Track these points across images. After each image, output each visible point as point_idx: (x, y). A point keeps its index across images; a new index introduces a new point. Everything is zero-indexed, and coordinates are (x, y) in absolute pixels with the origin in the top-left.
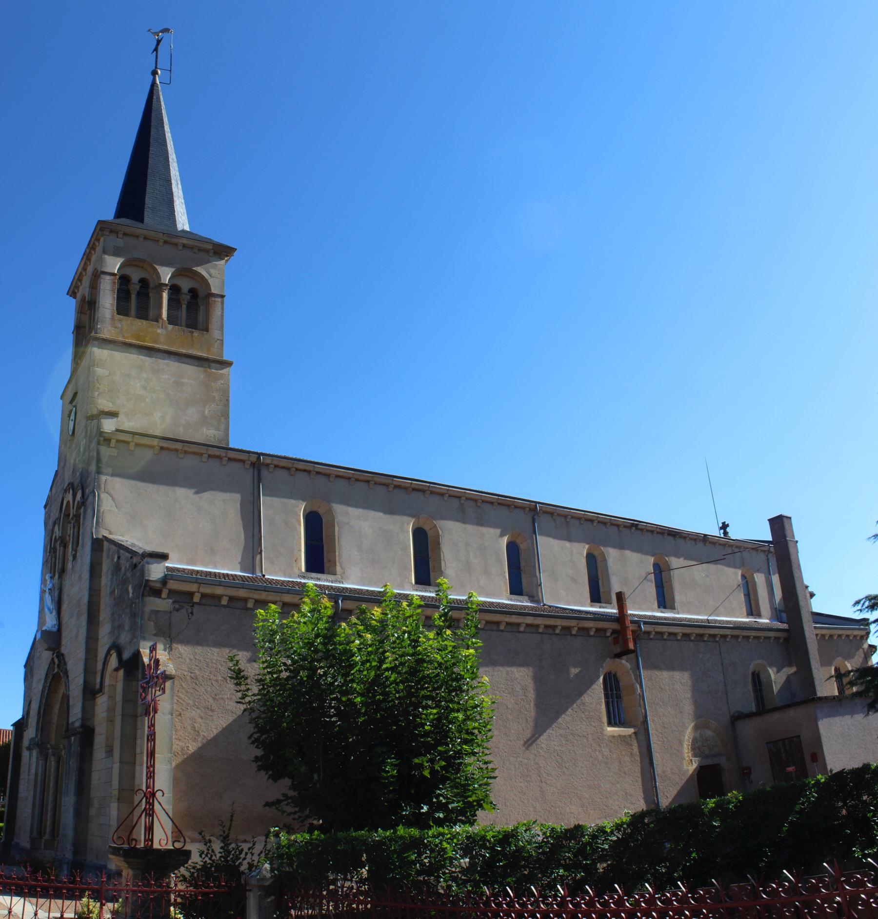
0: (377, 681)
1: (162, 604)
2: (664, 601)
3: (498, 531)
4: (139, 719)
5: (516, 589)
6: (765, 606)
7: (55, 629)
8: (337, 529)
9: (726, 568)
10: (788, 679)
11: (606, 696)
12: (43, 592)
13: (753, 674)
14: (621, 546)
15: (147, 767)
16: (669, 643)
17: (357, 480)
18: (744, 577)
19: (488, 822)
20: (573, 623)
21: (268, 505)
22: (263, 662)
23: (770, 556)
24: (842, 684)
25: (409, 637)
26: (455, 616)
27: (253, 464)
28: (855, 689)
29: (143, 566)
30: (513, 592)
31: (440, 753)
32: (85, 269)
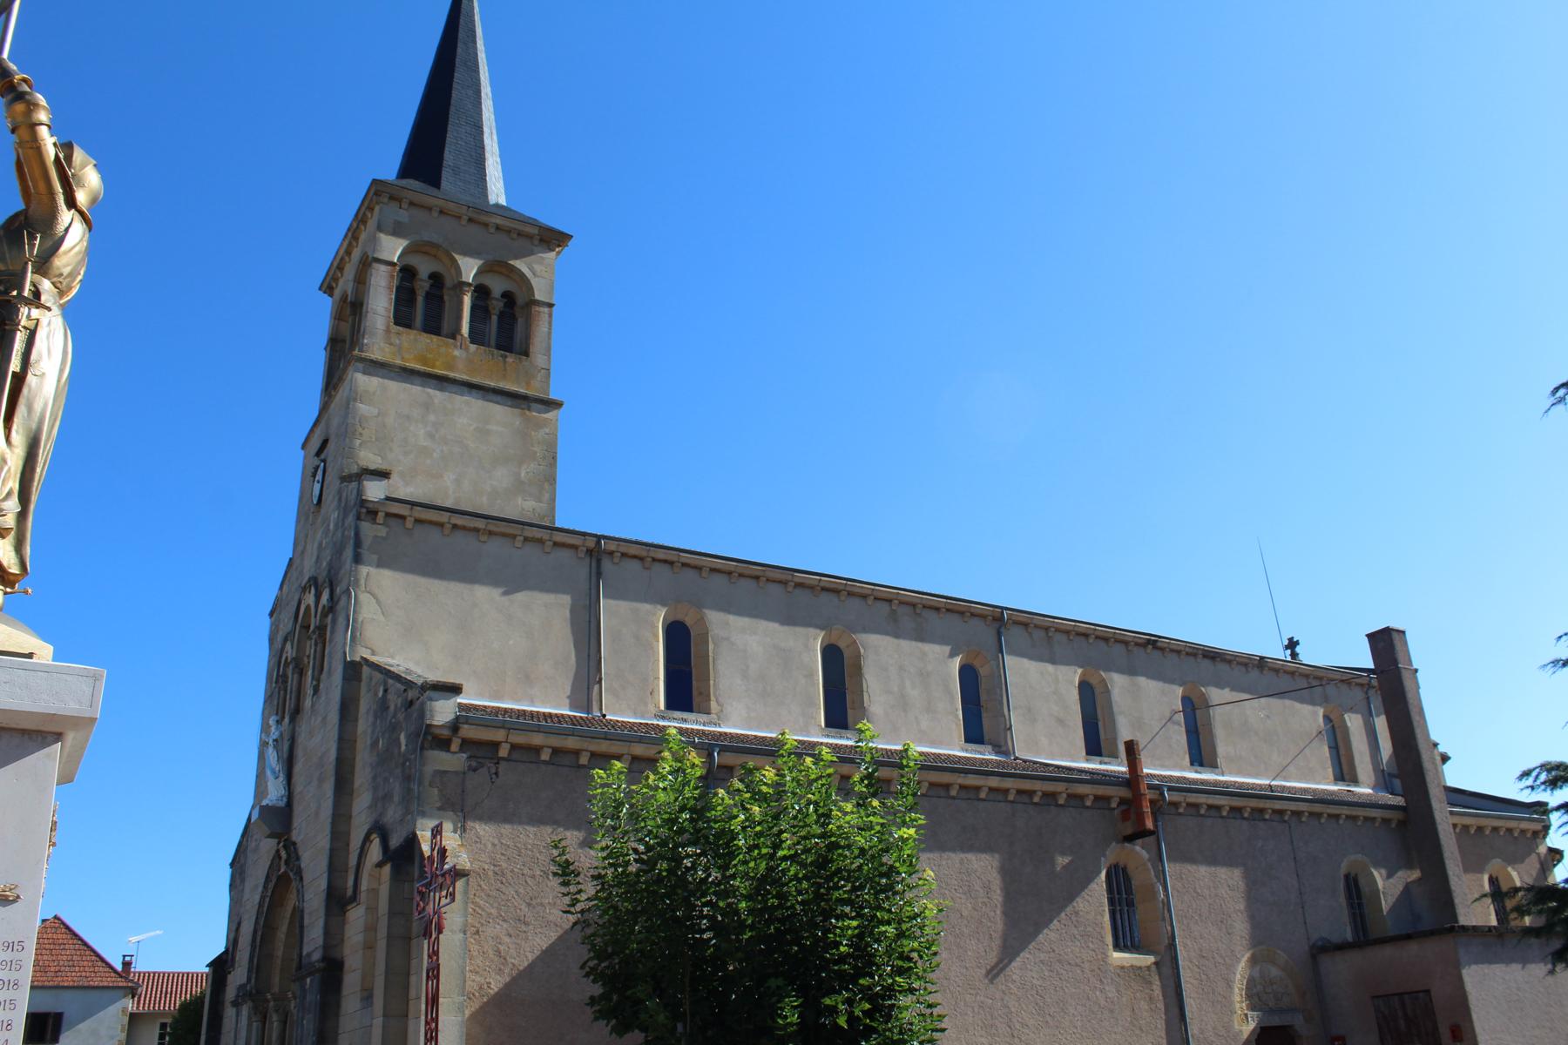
0: (770, 879)
1: (451, 761)
2: (1201, 754)
3: (947, 649)
4: (414, 942)
5: (974, 735)
6: (1364, 767)
7: (282, 804)
8: (711, 647)
9: (1298, 705)
11: (1111, 902)
12: (263, 745)
13: (1347, 877)
14: (1131, 671)
15: (427, 1023)
16: (1208, 822)
17: (741, 575)
18: (1327, 718)
20: (1060, 787)
21: (611, 612)
22: (603, 849)
23: (1371, 692)
24: (1504, 907)
25: (816, 811)
26: (884, 777)
27: (590, 552)
28: (1527, 920)
29: (423, 704)
31: (863, 989)
32: (348, 252)
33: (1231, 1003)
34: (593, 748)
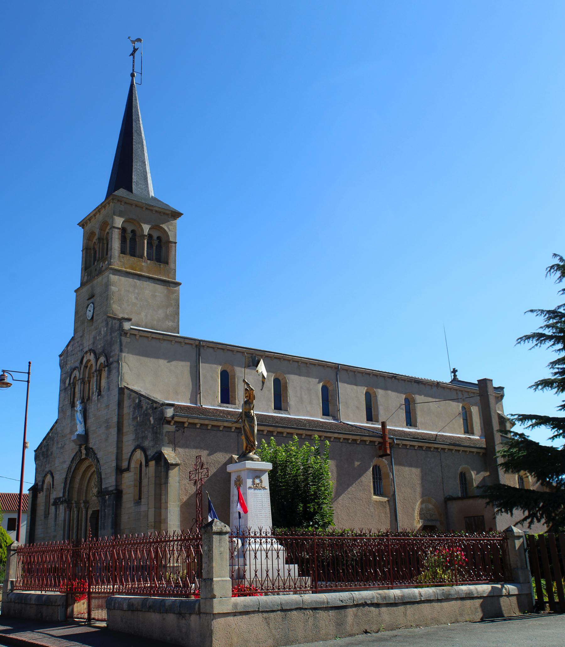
1: (170, 428)
2: (411, 421)
3: (318, 380)
5: (326, 413)
7: (84, 433)
8: (236, 380)
10: (484, 478)
11: (374, 478)
13: (461, 473)
14: (386, 388)
16: (410, 451)
18: (463, 408)
20: (358, 438)
21: (204, 368)
27: (196, 346)
33: (414, 516)
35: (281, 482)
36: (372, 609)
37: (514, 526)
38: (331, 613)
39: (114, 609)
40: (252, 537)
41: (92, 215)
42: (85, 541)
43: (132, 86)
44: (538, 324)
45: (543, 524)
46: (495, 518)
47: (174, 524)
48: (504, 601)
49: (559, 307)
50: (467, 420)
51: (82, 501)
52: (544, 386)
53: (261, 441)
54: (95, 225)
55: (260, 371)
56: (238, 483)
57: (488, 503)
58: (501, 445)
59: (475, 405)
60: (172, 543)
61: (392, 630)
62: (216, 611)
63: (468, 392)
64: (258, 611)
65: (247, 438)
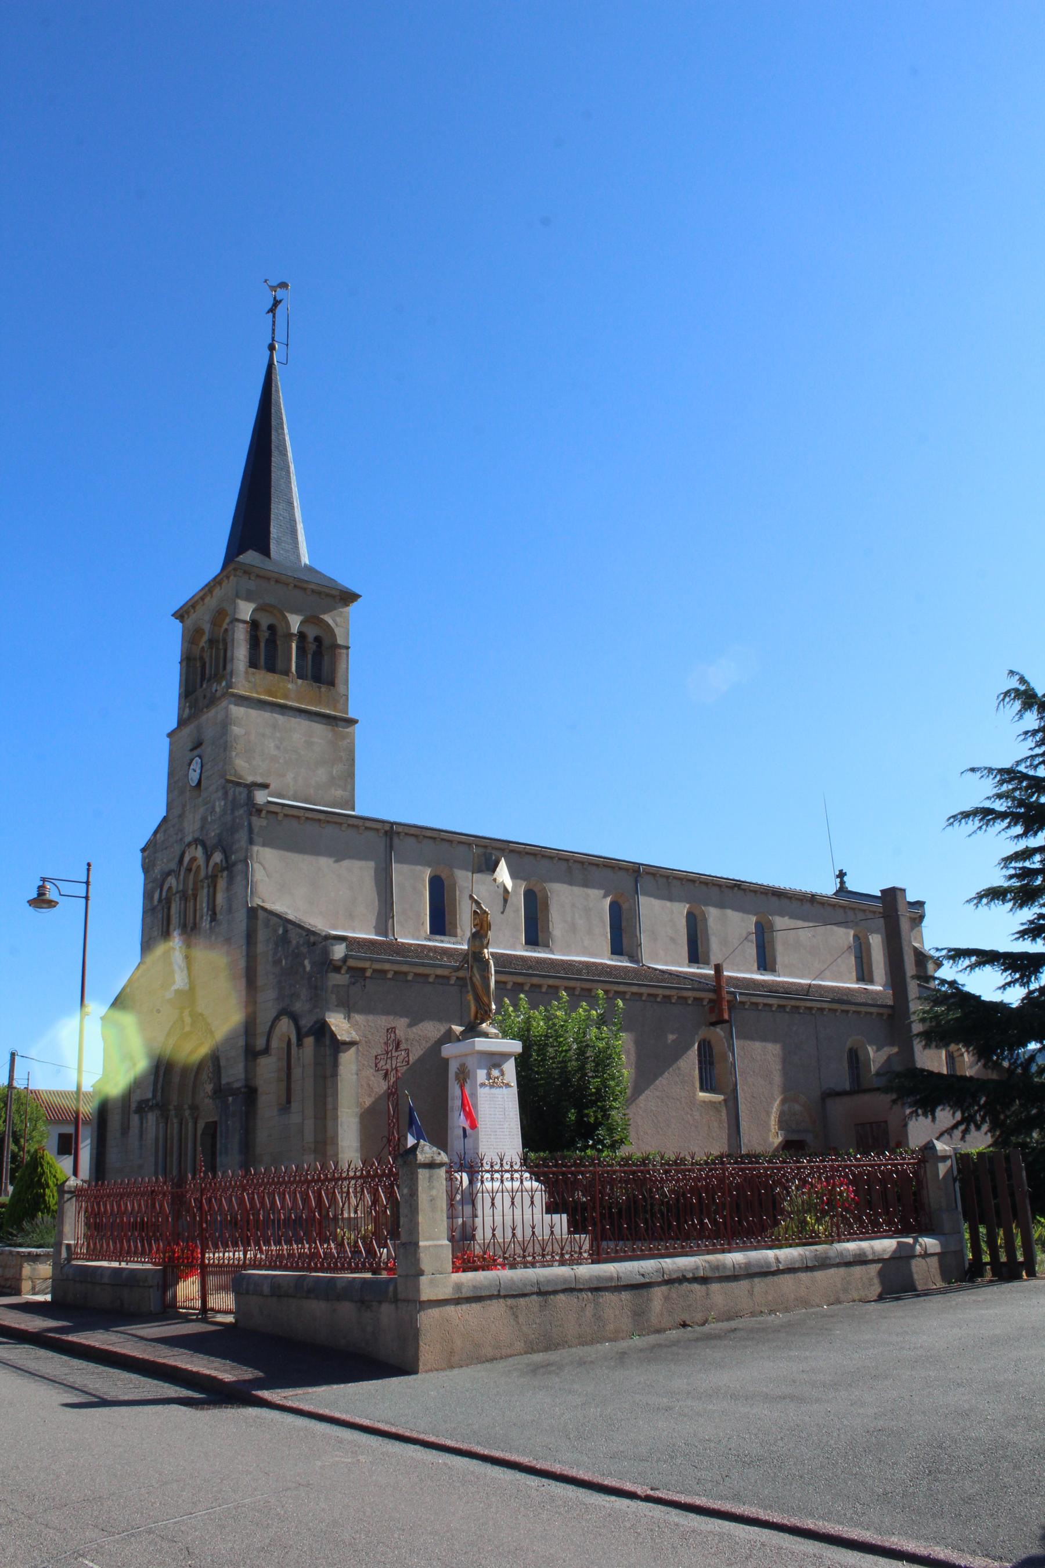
2: (765, 963)
3: (602, 892)
5: (617, 950)
7: (187, 988)
8: (458, 893)
11: (700, 1062)
13: (851, 1050)
14: (721, 905)
18: (856, 937)
19: (623, 1152)
20: (673, 992)
21: (399, 871)
27: (386, 832)
30: (613, 952)
34: (415, 971)
35: (537, 1073)
36: (696, 1286)
37: (938, 1139)
38: (625, 1295)
39: (247, 1293)
40: (488, 1171)
41: (196, 598)
42: (194, 1178)
43: (270, 366)
44: (983, 792)
45: (986, 1134)
46: (906, 1125)
47: (349, 1147)
48: (918, 1267)
49: (1018, 763)
50: (861, 958)
51: (186, 1106)
52: (992, 899)
53: (502, 1001)
54: (203, 616)
55: (499, 880)
56: (461, 1076)
57: (894, 1102)
58: (918, 1001)
59: (876, 931)
60: (346, 1183)
61: (729, 1319)
62: (424, 1297)
63: (864, 911)
64: (498, 1296)
65: (478, 999)
